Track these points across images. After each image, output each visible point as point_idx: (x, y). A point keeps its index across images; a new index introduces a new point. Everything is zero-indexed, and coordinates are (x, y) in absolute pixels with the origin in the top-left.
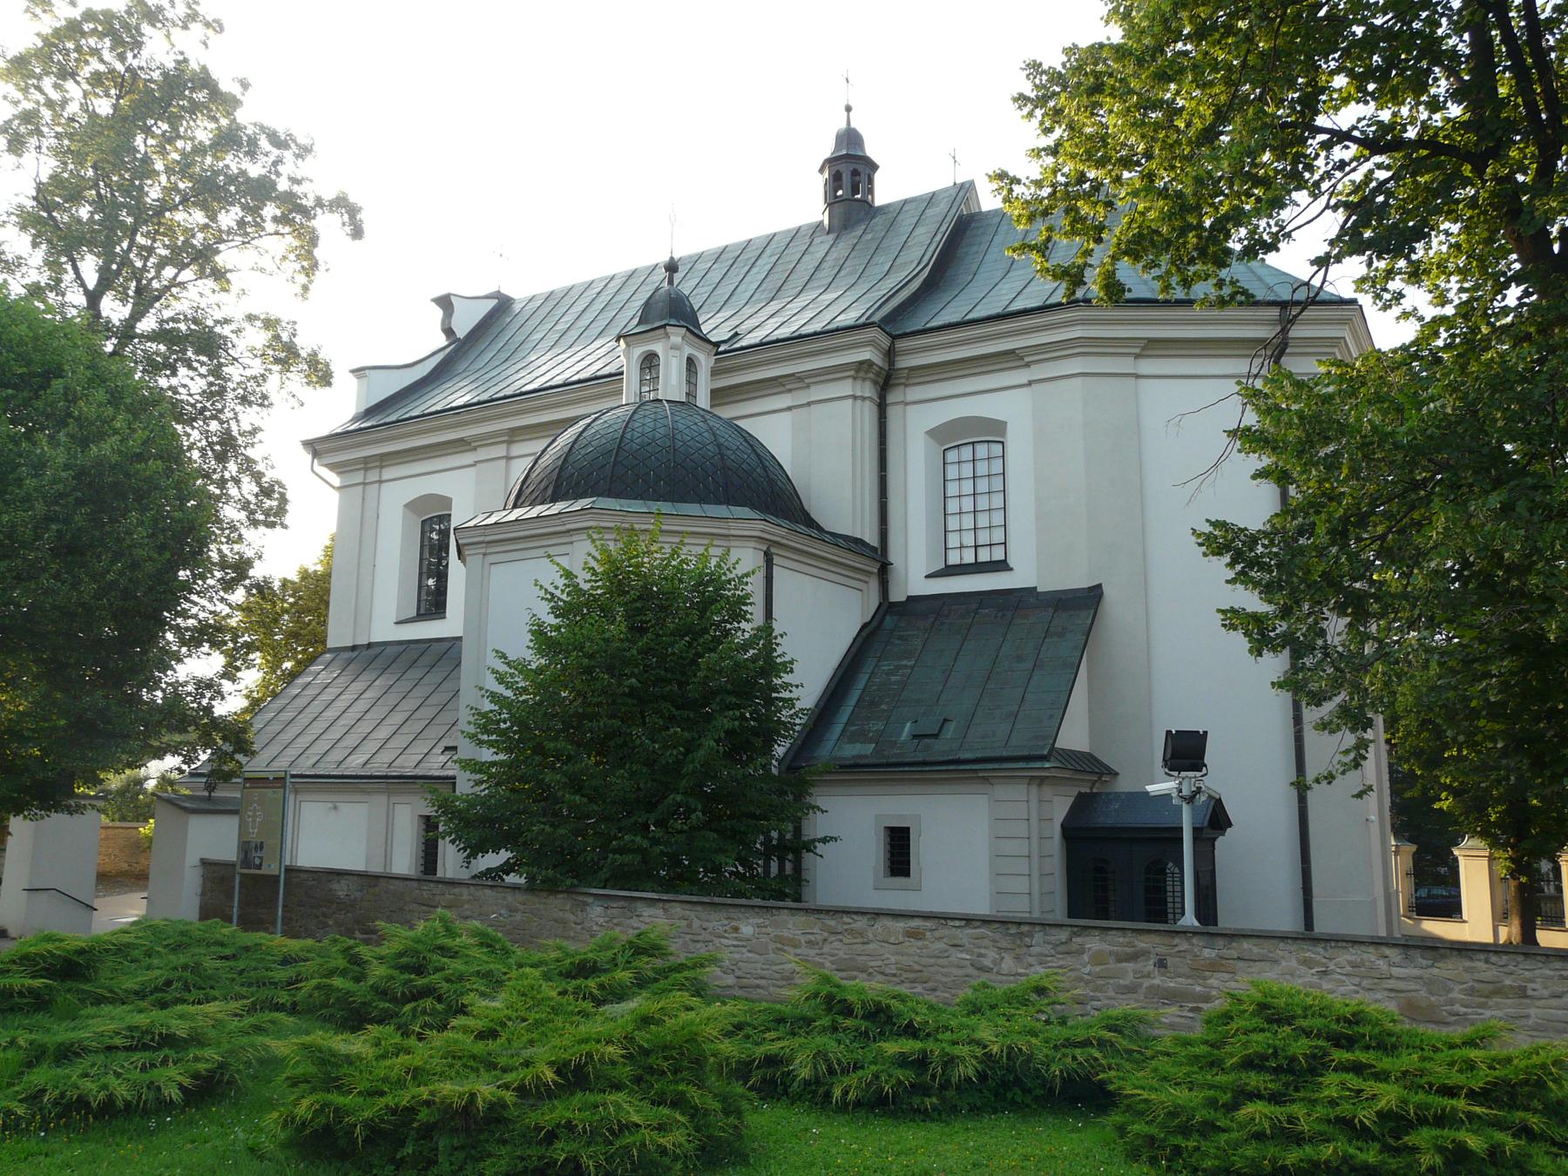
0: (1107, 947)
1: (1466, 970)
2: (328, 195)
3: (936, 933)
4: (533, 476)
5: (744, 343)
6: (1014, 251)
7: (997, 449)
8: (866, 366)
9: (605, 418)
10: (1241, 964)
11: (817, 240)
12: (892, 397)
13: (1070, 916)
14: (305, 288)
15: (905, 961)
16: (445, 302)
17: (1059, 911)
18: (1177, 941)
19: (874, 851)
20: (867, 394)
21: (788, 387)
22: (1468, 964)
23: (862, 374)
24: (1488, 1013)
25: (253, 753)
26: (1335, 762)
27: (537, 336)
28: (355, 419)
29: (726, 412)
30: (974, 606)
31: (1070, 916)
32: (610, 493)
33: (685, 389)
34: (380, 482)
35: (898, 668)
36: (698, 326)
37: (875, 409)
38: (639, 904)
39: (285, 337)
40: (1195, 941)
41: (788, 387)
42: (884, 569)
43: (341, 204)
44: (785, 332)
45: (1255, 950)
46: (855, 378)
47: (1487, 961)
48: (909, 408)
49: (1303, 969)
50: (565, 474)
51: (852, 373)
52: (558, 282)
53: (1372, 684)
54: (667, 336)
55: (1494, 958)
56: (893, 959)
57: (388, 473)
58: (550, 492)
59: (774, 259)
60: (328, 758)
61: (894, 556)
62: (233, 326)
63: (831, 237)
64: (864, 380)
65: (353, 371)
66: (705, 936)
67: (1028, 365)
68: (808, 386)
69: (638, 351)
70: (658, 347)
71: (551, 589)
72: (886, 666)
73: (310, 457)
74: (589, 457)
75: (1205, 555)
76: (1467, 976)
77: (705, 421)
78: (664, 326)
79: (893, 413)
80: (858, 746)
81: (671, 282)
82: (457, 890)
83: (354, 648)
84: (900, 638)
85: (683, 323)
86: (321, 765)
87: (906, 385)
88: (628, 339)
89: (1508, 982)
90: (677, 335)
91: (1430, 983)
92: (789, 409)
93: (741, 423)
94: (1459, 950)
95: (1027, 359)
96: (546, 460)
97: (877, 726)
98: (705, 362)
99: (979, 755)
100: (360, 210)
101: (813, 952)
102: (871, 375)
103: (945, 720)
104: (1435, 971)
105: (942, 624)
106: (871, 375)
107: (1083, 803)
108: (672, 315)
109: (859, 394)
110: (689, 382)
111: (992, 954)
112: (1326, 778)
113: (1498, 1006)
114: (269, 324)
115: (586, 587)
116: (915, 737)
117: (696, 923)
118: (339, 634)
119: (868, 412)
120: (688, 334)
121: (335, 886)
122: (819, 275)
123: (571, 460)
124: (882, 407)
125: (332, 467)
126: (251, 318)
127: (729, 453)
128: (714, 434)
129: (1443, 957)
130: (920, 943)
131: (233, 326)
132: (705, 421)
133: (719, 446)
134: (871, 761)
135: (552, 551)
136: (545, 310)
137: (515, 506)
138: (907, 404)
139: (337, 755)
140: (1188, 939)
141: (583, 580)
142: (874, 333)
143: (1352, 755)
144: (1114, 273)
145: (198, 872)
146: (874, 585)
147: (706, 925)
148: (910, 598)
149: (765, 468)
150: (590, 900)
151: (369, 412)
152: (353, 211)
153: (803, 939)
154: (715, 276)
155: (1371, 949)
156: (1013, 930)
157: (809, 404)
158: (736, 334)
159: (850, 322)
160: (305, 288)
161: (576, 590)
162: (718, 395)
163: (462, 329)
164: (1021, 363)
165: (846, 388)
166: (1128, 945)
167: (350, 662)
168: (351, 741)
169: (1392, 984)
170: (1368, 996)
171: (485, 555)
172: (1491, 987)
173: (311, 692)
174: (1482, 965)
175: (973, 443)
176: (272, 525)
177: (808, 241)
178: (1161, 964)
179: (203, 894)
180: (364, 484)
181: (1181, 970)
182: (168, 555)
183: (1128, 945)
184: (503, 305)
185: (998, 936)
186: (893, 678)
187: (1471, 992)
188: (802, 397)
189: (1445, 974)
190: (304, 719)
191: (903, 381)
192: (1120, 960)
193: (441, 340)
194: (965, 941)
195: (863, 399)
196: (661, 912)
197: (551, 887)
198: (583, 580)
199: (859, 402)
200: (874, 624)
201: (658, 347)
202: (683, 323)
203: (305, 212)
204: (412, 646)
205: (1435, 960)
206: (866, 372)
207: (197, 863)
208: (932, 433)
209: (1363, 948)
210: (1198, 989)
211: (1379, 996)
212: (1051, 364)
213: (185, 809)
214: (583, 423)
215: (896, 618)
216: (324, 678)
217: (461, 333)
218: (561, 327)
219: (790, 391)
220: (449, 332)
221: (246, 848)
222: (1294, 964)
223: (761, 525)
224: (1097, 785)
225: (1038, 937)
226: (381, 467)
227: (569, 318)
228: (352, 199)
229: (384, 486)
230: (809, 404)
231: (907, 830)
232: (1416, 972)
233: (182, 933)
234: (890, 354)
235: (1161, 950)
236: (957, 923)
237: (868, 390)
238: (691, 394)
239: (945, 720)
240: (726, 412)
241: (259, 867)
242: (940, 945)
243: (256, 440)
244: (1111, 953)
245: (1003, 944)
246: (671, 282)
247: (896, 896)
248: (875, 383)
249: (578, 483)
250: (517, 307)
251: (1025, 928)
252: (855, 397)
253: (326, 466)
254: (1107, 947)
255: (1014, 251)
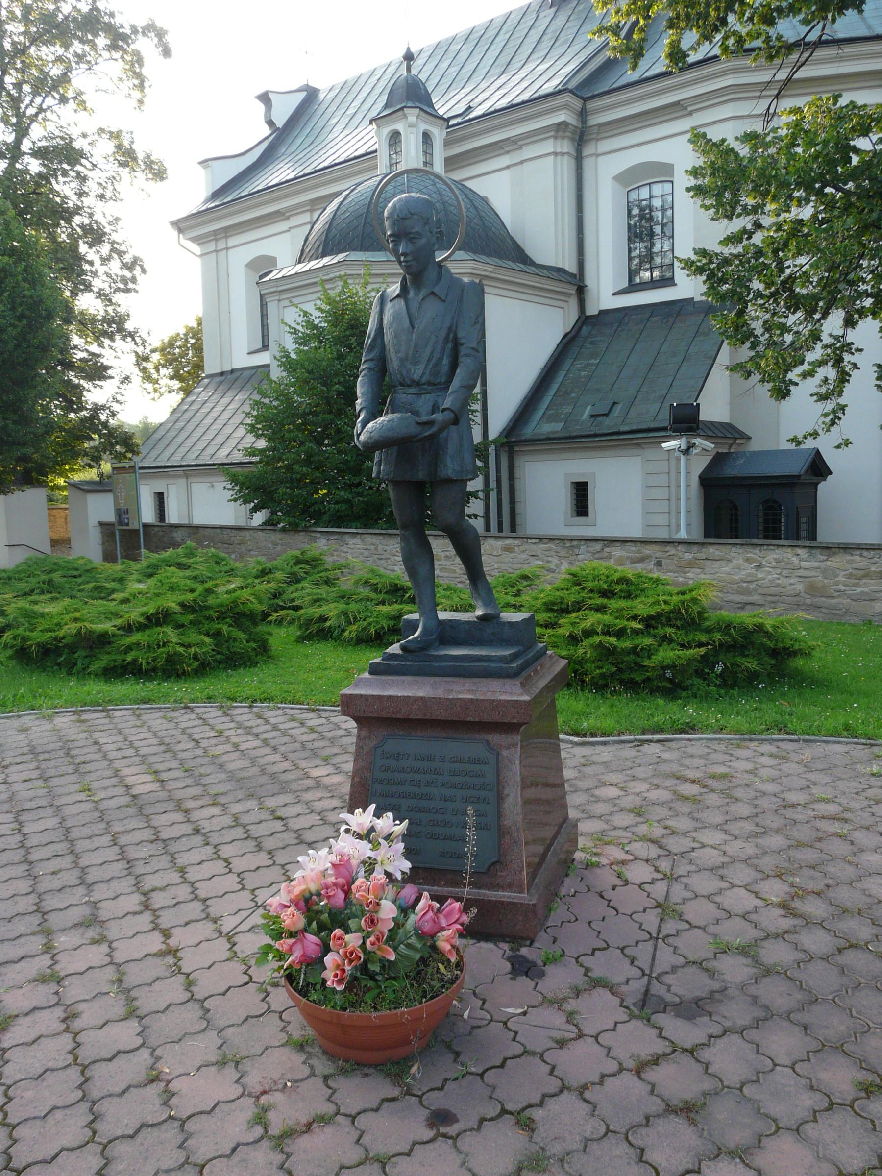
0: (624, 554)
1: (848, 562)
2: (141, 23)
3: (522, 548)
4: (310, 238)
5: (472, 116)
6: (594, 34)
7: (667, 187)
8: (563, 126)
9: (359, 189)
10: (708, 562)
11: (542, 15)
12: (588, 150)
13: (706, 536)
14: (141, 102)
15: (504, 567)
16: (265, 98)
17: (697, 534)
18: (668, 548)
19: (564, 499)
20: (565, 150)
21: (507, 149)
22: (849, 557)
23: (561, 134)
24: (859, 590)
25: (138, 453)
26: (820, 422)
27: (334, 121)
28: (206, 201)
29: (457, 176)
30: (647, 315)
31: (706, 536)
32: (363, 248)
33: (422, 159)
34: (227, 249)
35: (588, 365)
36: (431, 105)
37: (573, 162)
38: (346, 536)
39: (126, 143)
40: (679, 548)
41: (507, 149)
42: (581, 291)
43: (150, 28)
44: (526, 96)
45: (717, 553)
46: (555, 138)
47: (861, 555)
48: (600, 159)
49: (746, 564)
50: (331, 236)
51: (552, 133)
52: (350, 74)
53: (767, 366)
54: (405, 116)
55: (865, 553)
56: (496, 566)
57: (232, 242)
58: (320, 251)
59: (508, 36)
60: (205, 453)
61: (589, 281)
62: (89, 140)
63: (553, 9)
64: (563, 138)
65: (201, 163)
66: (386, 555)
67: (690, 114)
68: (521, 148)
69: (386, 131)
70: (400, 127)
71: (294, 325)
72: (578, 365)
73: (176, 233)
74: (347, 221)
75: (688, 276)
76: (848, 566)
77: (434, 184)
78: (402, 109)
79: (588, 163)
80: (553, 424)
81: (409, 69)
82: (243, 533)
83: (222, 374)
84: (592, 343)
85: (418, 104)
86: (201, 457)
87: (598, 140)
88: (379, 121)
89: (873, 569)
90: (412, 115)
91: (825, 572)
92: (508, 167)
93: (469, 184)
94: (844, 549)
95: (690, 109)
96: (318, 226)
97: (567, 409)
98: (438, 135)
99: (635, 427)
100: (166, 32)
101: (449, 563)
102: (568, 134)
103: (615, 403)
104: (829, 563)
105: (623, 330)
106: (568, 134)
107: (719, 460)
108: (409, 98)
109: (559, 150)
110: (425, 153)
111: (555, 561)
112: (811, 435)
113: (865, 585)
114: (116, 135)
115: (316, 322)
116: (592, 416)
117: (380, 547)
118: (211, 366)
119: (567, 165)
120: (422, 113)
121: (175, 535)
122: (539, 47)
123: (335, 224)
124: (579, 160)
125: (194, 240)
126: (101, 131)
127: (452, 208)
128: (440, 195)
129: (834, 554)
130: (512, 555)
131: (89, 140)
132: (434, 184)
133: (444, 203)
134: (559, 435)
135: (295, 301)
136: (341, 96)
137: (300, 262)
138: (598, 155)
139: (210, 451)
140: (675, 547)
141: (317, 317)
142: (567, 98)
143: (831, 416)
144: (679, 42)
145: (98, 530)
146: (574, 303)
147: (386, 548)
148: (602, 312)
149: (481, 218)
150: (318, 535)
151: (215, 195)
152: (160, 34)
153: (443, 555)
154: (463, 55)
155: (789, 550)
156: (568, 544)
157: (522, 162)
158: (470, 107)
159: (550, 90)
160: (141, 102)
161: (310, 324)
162: (451, 162)
163: (281, 117)
164: (685, 112)
165: (548, 146)
166: (639, 552)
167: (221, 383)
168: (220, 440)
169: (801, 573)
170: (786, 581)
171: (279, 301)
172: (862, 572)
173: (195, 407)
174: (858, 558)
175: (650, 184)
176: (127, 291)
177: (534, 16)
178: (659, 564)
179: (103, 544)
180: (216, 251)
181: (670, 568)
182: (25, 322)
183: (639, 552)
184: (311, 95)
185: (558, 549)
186: (583, 374)
187: (849, 576)
188: (516, 157)
189: (834, 565)
190: (191, 427)
191: (594, 136)
192: (633, 563)
193: (266, 131)
194: (539, 553)
195: (563, 154)
196: (359, 541)
197: (294, 528)
198: (317, 317)
199: (559, 157)
200: (573, 333)
201: (400, 127)
202: (418, 104)
203: (125, 38)
204: (260, 370)
205: (829, 556)
206: (564, 132)
207: (96, 524)
208: (618, 178)
209: (784, 549)
210: (681, 579)
211: (792, 581)
212: (709, 111)
213: (83, 490)
214: (344, 194)
215: (589, 328)
216: (204, 396)
217: (280, 124)
218: (351, 111)
219: (508, 152)
220: (270, 123)
221: (120, 513)
222: (741, 561)
223: (472, 264)
224: (734, 446)
225: (583, 548)
226: (226, 237)
227: (357, 103)
228: (159, 24)
229: (230, 252)
230: (522, 162)
231: (586, 484)
232: (816, 564)
233: (55, 564)
234: (583, 114)
235: (658, 554)
236: (534, 541)
237: (566, 146)
238: (428, 163)
239: (615, 403)
240: (457, 176)
241: (128, 525)
242: (524, 556)
243: (118, 227)
244: (627, 558)
245: (563, 553)
246: (409, 69)
247: (580, 528)
248: (572, 140)
249: (339, 242)
250: (321, 96)
251: (575, 543)
252: (555, 154)
253: (190, 239)
254: (624, 554)
255: (594, 34)
